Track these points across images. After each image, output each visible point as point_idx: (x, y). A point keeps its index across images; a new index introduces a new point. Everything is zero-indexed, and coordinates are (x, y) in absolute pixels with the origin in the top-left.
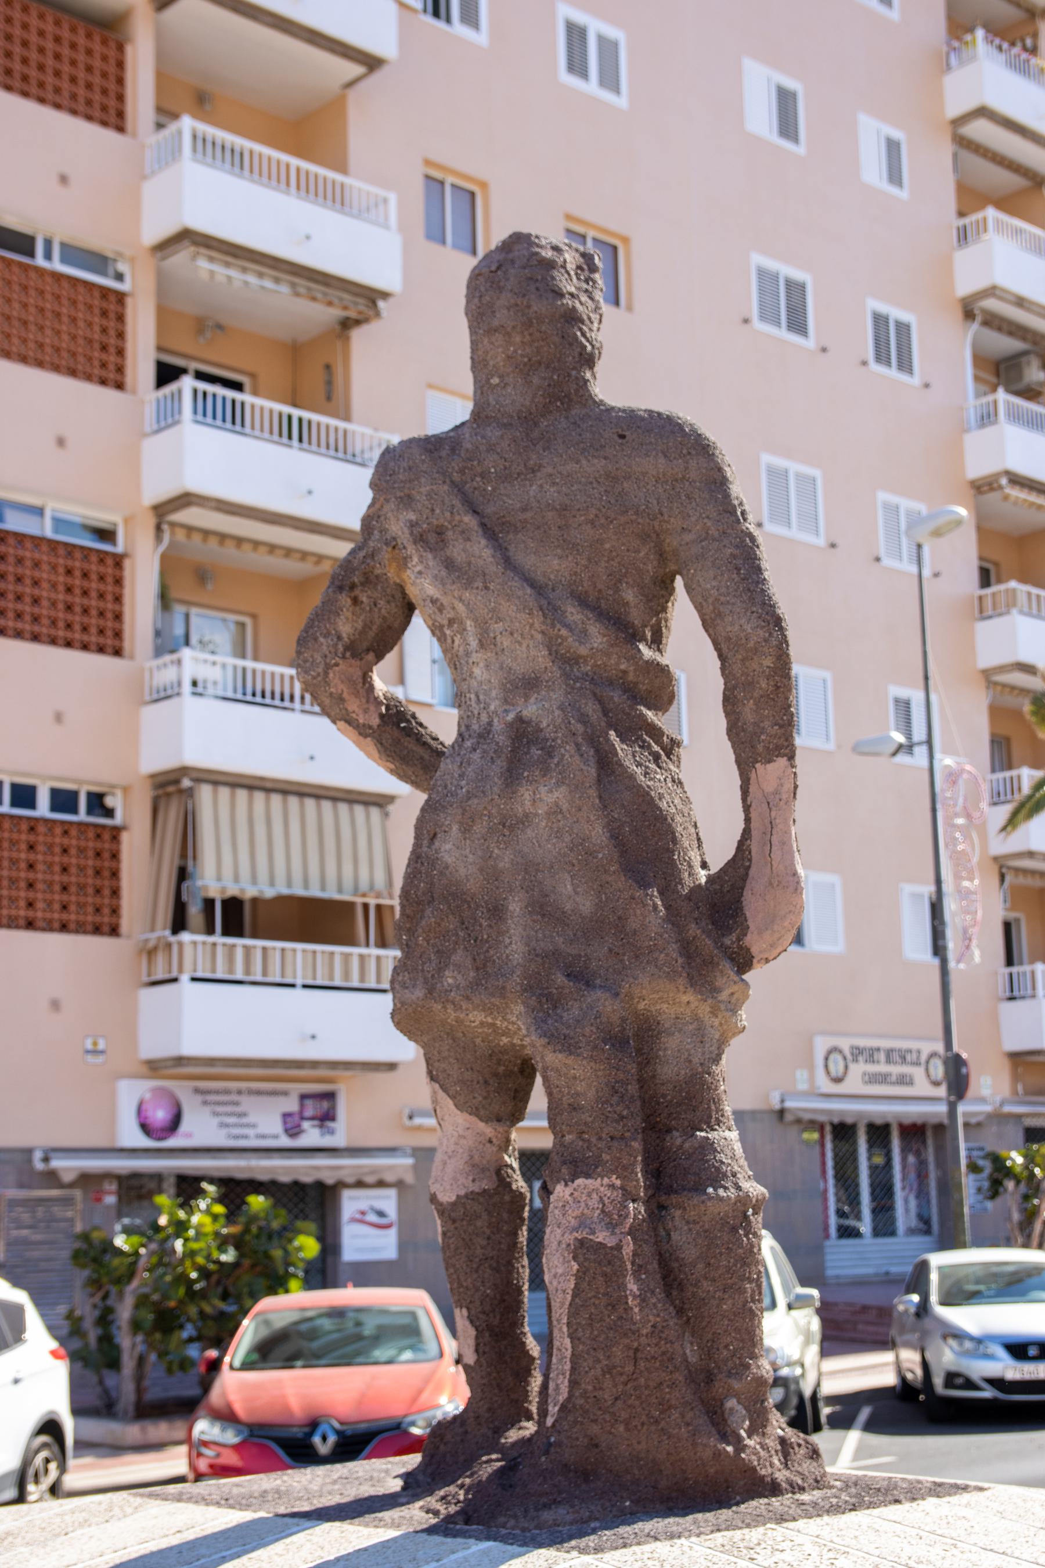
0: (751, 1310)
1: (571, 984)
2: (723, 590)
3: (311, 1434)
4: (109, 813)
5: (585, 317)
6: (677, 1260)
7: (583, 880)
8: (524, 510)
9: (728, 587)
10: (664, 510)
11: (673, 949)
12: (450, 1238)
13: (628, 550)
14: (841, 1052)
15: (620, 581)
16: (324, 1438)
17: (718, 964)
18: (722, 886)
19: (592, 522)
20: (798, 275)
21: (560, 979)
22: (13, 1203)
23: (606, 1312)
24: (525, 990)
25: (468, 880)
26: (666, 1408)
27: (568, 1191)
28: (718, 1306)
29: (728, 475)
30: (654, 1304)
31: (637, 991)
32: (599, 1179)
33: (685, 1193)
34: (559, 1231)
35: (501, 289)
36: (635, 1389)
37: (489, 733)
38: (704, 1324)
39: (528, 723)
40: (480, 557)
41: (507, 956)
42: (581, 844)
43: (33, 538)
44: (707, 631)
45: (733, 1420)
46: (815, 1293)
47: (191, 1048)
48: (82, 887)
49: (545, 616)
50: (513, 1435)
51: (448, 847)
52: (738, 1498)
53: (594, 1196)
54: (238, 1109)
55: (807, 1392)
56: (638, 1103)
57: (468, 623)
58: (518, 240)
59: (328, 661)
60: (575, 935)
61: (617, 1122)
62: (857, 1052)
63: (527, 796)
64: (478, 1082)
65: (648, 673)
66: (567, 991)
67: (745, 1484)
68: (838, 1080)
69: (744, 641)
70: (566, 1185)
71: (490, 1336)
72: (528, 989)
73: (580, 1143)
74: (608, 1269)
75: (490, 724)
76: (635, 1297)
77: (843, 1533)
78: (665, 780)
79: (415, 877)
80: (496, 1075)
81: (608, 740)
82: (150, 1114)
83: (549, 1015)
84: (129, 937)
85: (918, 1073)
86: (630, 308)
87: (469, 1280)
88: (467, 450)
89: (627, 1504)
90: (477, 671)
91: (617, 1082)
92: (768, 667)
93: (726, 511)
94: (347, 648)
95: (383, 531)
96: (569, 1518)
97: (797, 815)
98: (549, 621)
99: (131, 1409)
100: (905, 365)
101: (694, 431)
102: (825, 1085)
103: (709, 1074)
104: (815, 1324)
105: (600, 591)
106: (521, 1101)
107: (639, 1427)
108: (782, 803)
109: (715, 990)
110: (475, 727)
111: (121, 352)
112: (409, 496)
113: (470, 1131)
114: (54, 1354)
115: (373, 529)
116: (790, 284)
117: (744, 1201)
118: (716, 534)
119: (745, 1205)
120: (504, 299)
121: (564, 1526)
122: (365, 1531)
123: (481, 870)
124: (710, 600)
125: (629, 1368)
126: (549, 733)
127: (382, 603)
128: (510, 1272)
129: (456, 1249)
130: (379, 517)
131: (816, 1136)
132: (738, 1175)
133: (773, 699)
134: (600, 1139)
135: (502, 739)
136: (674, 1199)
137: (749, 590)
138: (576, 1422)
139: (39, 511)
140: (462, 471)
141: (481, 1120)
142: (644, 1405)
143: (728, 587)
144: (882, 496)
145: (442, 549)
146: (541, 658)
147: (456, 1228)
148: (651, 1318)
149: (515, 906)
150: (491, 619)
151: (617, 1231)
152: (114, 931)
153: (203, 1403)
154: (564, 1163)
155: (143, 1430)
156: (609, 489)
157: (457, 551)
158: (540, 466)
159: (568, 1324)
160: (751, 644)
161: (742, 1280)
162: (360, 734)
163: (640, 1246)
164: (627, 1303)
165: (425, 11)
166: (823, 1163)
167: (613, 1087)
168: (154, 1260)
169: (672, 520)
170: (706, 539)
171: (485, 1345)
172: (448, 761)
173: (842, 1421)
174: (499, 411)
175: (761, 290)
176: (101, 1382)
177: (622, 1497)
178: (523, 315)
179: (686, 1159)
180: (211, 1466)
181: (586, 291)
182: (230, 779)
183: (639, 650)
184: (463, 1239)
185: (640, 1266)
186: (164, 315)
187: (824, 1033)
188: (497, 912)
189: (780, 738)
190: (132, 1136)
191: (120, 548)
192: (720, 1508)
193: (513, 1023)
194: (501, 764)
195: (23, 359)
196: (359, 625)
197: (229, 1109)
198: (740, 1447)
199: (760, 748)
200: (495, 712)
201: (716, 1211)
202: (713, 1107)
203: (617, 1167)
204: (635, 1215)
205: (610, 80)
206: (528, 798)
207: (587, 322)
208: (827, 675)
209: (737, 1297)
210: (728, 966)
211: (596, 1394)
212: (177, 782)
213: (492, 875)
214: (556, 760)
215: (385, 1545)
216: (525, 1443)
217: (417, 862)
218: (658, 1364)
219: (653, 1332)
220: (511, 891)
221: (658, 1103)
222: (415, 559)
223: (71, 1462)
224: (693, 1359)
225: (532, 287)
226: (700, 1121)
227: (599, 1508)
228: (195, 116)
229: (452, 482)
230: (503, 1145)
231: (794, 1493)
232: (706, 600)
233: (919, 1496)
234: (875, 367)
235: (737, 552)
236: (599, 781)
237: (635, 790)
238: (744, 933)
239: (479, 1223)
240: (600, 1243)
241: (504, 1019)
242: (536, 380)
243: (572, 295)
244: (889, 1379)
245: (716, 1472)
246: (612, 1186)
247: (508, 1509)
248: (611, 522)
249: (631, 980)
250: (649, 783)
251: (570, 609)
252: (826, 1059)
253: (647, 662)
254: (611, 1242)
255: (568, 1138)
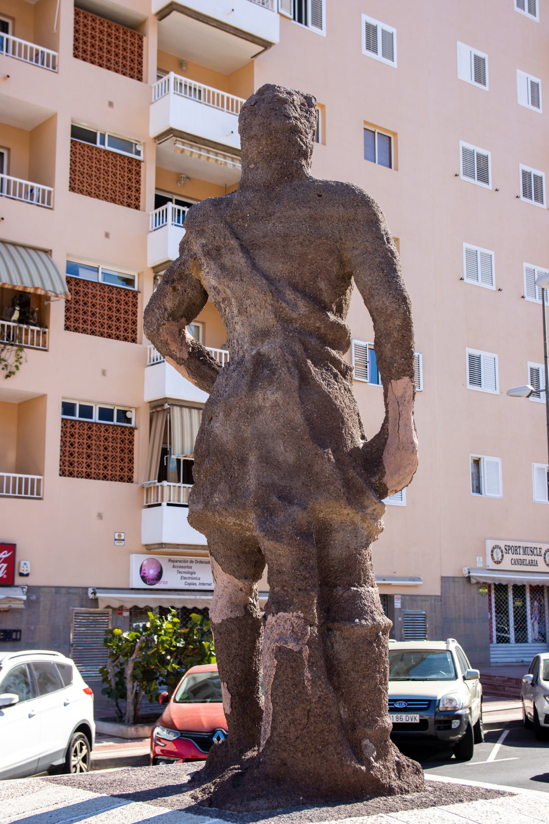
0: (379, 689)
1: (280, 502)
2: (374, 282)
3: (212, 736)
4: (129, 421)
5: (303, 131)
6: (337, 660)
7: (290, 444)
8: (264, 237)
9: (377, 280)
10: (343, 237)
11: (339, 484)
12: (218, 643)
13: (321, 259)
14: (500, 548)
15: (317, 277)
16: (219, 739)
17: (366, 492)
18: (371, 449)
19: (301, 243)
20: (484, 152)
21: (275, 499)
22: (77, 614)
23: (292, 689)
24: (256, 505)
25: (228, 443)
26: (325, 744)
27: (274, 619)
28: (360, 686)
29: (380, 218)
30: (320, 685)
31: (317, 507)
32: (291, 613)
33: (342, 622)
34: (269, 642)
35: (256, 115)
36: (308, 733)
37: (243, 361)
38: (351, 696)
39: (264, 356)
40: (239, 263)
41: (248, 486)
42: (289, 424)
43: (93, 282)
44: (366, 305)
45: (366, 752)
46: (478, 671)
47: (166, 539)
48: (114, 458)
49: (273, 296)
50: (250, 754)
51: (218, 425)
52: (368, 796)
53: (288, 622)
54: (190, 570)
55: (473, 724)
56: (317, 571)
57: (233, 300)
58: (268, 88)
59: (159, 322)
60: (284, 475)
61: (303, 580)
62: (508, 549)
63: (260, 396)
64: (234, 557)
65: (333, 329)
66: (278, 506)
67: (373, 788)
68: (498, 562)
69: (385, 310)
70: (273, 616)
71: (239, 698)
72: (257, 505)
73: (283, 592)
74: (294, 664)
75: (244, 357)
76: (309, 680)
77: (423, 820)
78: (340, 389)
79: (201, 441)
80: (244, 553)
81: (306, 365)
82: (146, 571)
83: (267, 519)
84: (137, 483)
85: (540, 560)
86: (396, 169)
87: (228, 667)
88: (235, 204)
89: (301, 798)
90: (238, 327)
91: (303, 558)
92: (398, 325)
93: (377, 238)
94: (170, 315)
95: (190, 250)
96: (266, 806)
97: (415, 409)
98: (275, 298)
99: (131, 719)
100: (539, 198)
101: (361, 192)
102: (492, 565)
103: (360, 555)
104: (479, 687)
105: (305, 282)
106: (258, 568)
107: (310, 755)
108: (405, 402)
109: (363, 507)
110: (236, 358)
111: (138, 190)
112: (203, 230)
113: (230, 584)
114: (85, 691)
115: (185, 249)
116: (479, 156)
117: (377, 627)
118: (371, 250)
119: (377, 629)
120: (257, 121)
121: (262, 811)
122: (153, 808)
123: (235, 438)
124: (367, 288)
125: (304, 721)
126: (274, 361)
127: (189, 290)
128: (251, 663)
129: (222, 649)
130: (188, 242)
131: (486, 590)
132: (374, 613)
133: (401, 343)
134: (293, 590)
135: (249, 365)
136: (336, 625)
137: (388, 281)
138: (274, 751)
139: (96, 270)
140: (231, 216)
141: (236, 578)
142: (313, 742)
143: (377, 280)
144: (526, 265)
145: (219, 259)
146: (271, 319)
147: (221, 638)
148: (318, 692)
149: (252, 458)
150: (244, 297)
151: (300, 643)
152: (130, 480)
153: (160, 719)
154: (273, 603)
155: (136, 729)
156: (311, 225)
157: (227, 260)
158: (274, 212)
159: (272, 695)
160: (389, 312)
161: (374, 672)
162: (178, 363)
163: (314, 651)
164: (304, 684)
165: (294, 19)
166: (490, 605)
167: (301, 561)
168: (144, 645)
169: (347, 242)
170: (366, 253)
171: (236, 703)
172: (220, 377)
173: (492, 738)
174: (254, 183)
175: (465, 159)
176: (117, 705)
177: (298, 795)
178: (267, 129)
179: (344, 602)
180: (162, 751)
181: (306, 117)
182: (189, 405)
183: (327, 316)
184: (225, 644)
185: (313, 663)
186: (159, 172)
187: (491, 538)
188: (243, 461)
189: (405, 365)
190: (138, 583)
191: (136, 289)
192: (356, 802)
193: (251, 524)
194: (247, 378)
195: (89, 194)
196: (177, 302)
197: (186, 570)
198: (370, 767)
199: (393, 371)
200: (247, 350)
201: (360, 633)
202: (362, 573)
203: (301, 606)
204: (311, 634)
205: (389, 53)
206: (261, 397)
207: (304, 133)
208: (496, 356)
209: (371, 682)
210: (371, 494)
211: (286, 735)
212: (163, 405)
213: (241, 441)
214: (276, 376)
215: (160, 817)
216: (252, 759)
217: (202, 433)
218: (321, 719)
219: (319, 701)
220: (251, 449)
221: (330, 570)
222: (205, 265)
223: (94, 745)
224: (344, 716)
225: (273, 113)
226: (354, 581)
227: (284, 800)
228: (175, 73)
229: (226, 222)
230: (248, 592)
231: (402, 794)
232: (365, 288)
233: (474, 798)
234: (522, 198)
235: (382, 260)
236: (300, 388)
237: (321, 394)
238: (383, 474)
239: (234, 636)
240: (290, 649)
241: (246, 522)
242: (274, 165)
243: (296, 118)
244: (519, 716)
245: (355, 781)
246: (298, 617)
247: (232, 799)
248: (312, 243)
249: (314, 500)
250: (329, 390)
251: (288, 292)
252: (492, 551)
253: (332, 322)
254: (296, 649)
255: (277, 589)
